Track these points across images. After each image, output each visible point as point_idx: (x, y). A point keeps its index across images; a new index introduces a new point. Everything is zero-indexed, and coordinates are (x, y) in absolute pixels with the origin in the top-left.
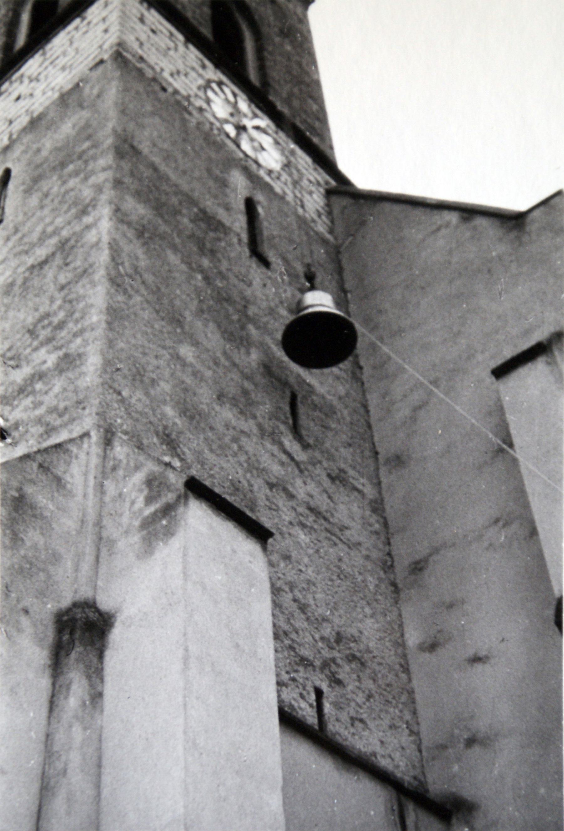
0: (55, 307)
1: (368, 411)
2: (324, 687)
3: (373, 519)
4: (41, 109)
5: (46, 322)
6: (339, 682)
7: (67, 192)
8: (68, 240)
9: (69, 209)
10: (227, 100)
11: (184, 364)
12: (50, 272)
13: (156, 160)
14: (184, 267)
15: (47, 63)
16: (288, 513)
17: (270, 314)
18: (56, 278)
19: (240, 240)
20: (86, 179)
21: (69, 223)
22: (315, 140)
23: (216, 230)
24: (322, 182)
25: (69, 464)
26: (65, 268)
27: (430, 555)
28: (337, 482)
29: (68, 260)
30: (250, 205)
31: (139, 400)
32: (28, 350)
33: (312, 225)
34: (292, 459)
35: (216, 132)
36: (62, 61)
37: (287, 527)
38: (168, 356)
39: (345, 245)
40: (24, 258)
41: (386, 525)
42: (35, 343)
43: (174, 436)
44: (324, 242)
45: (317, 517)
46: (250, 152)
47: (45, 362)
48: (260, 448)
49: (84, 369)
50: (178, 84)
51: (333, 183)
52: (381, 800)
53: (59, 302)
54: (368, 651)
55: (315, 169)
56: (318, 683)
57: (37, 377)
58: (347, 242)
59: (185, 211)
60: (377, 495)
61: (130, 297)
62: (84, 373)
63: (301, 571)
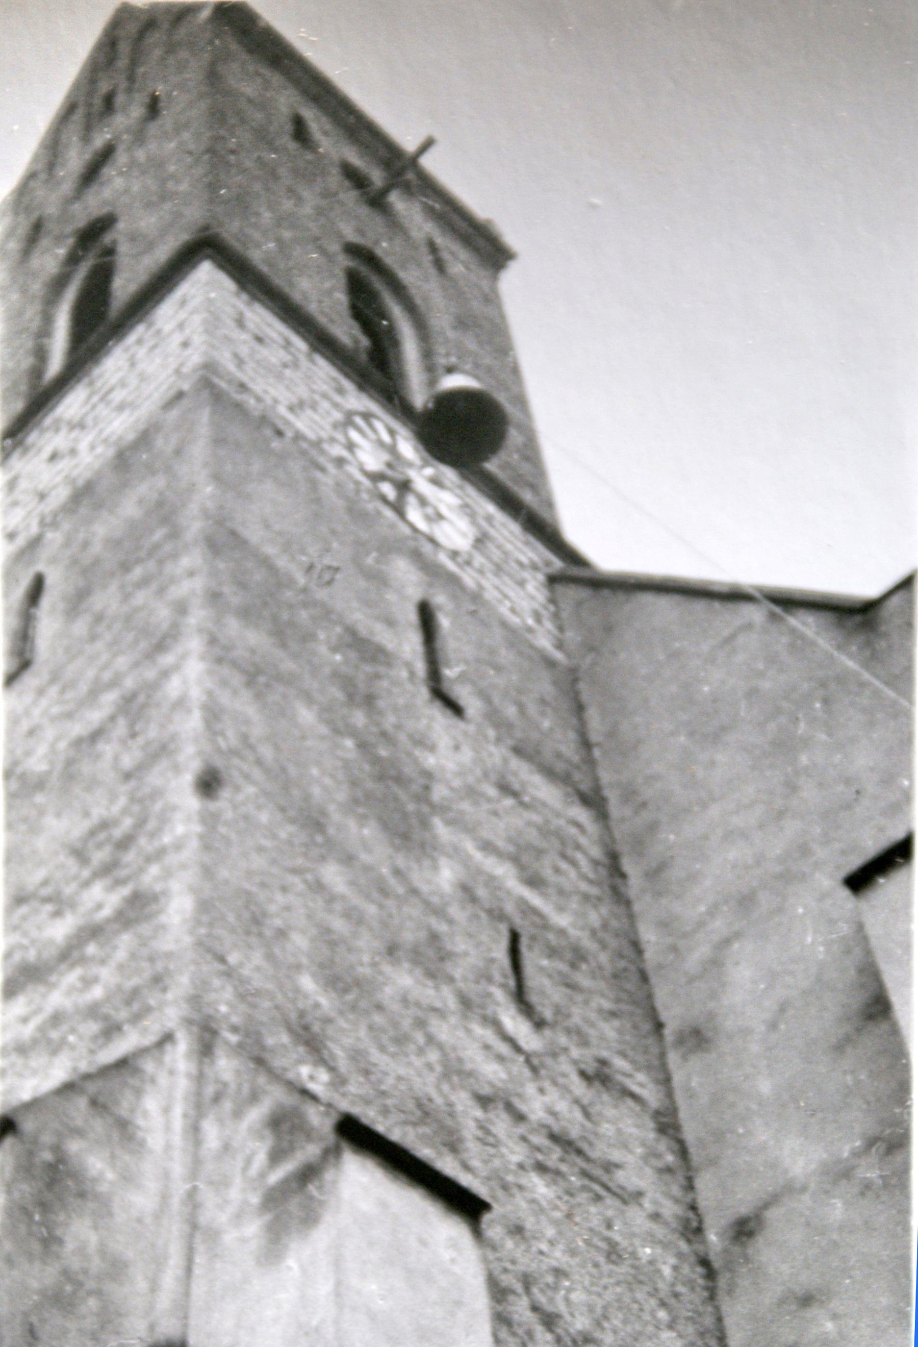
0: (116, 809)
3: (663, 1146)
4: (88, 475)
9: (136, 642)
10: (381, 443)
11: (332, 899)
12: (107, 749)
13: (270, 550)
14: (324, 730)
15: (95, 399)
19: (412, 674)
23: (373, 659)
24: (540, 563)
27: (766, 1206)
28: (597, 1084)
29: (137, 728)
31: (258, 969)
33: (529, 636)
34: (517, 1049)
35: (365, 496)
36: (118, 396)
37: (516, 1174)
41: (683, 1152)
44: (550, 664)
45: (566, 1152)
46: (422, 525)
47: (99, 906)
48: (461, 1033)
50: (302, 424)
53: (123, 801)
55: (527, 543)
59: (322, 636)
60: (667, 1102)
63: (541, 1253)
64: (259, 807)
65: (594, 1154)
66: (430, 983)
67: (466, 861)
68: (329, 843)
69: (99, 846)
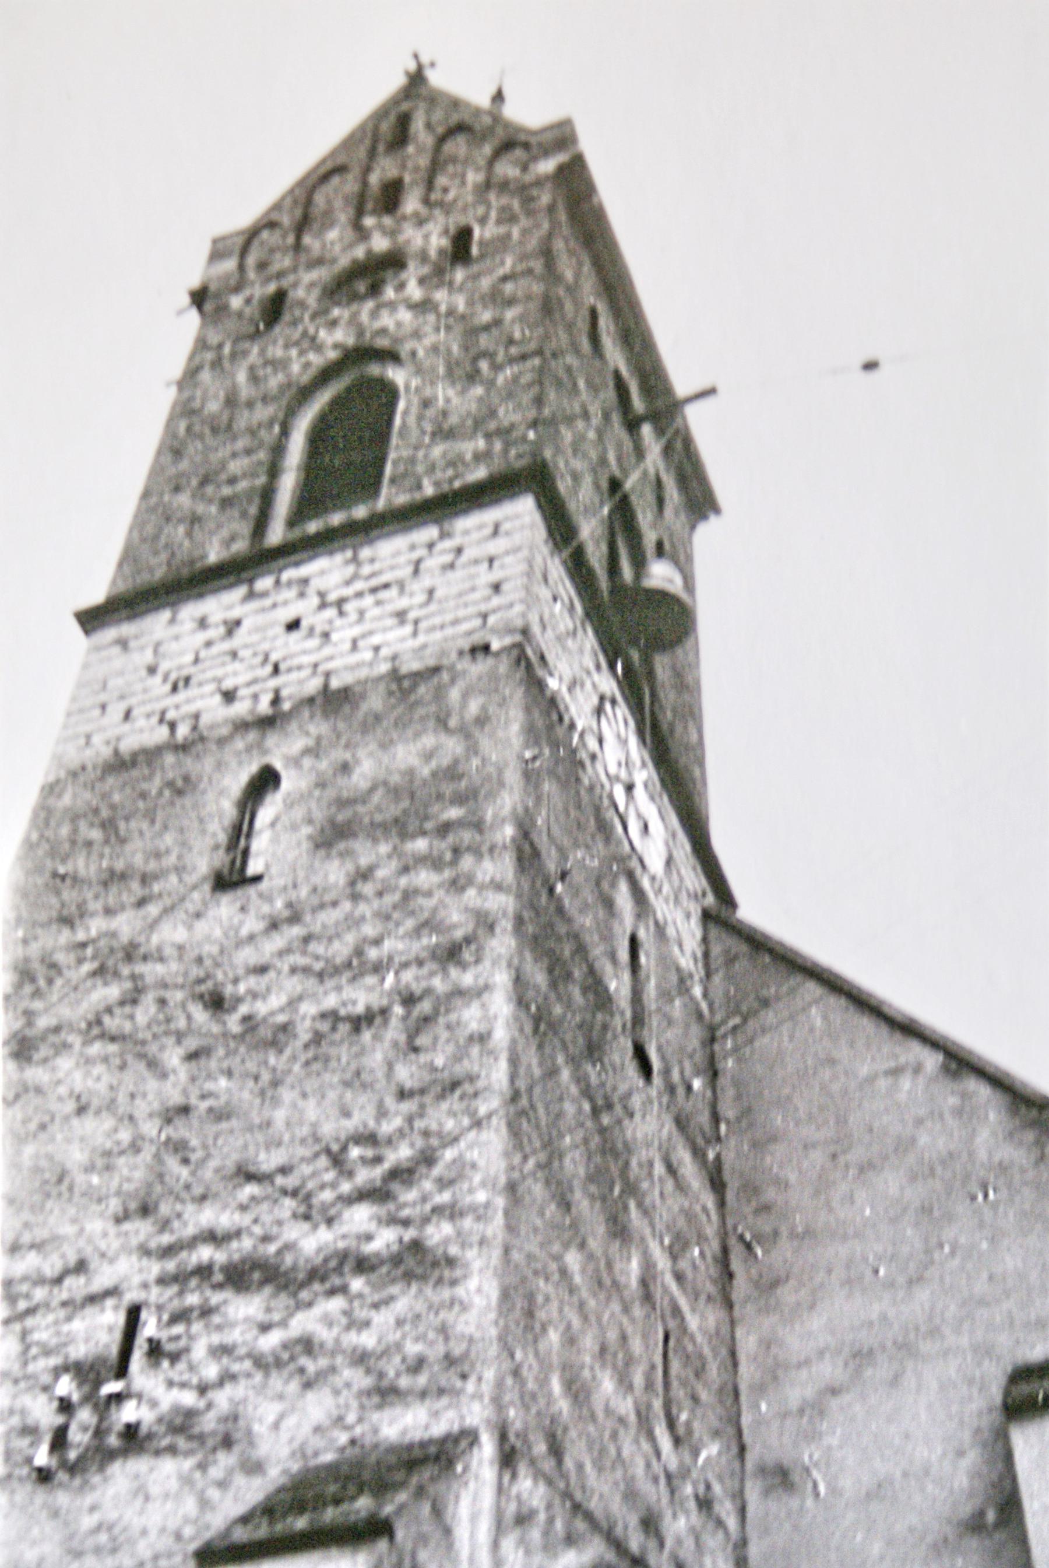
1: (735, 1364)
42: (346, 1187)
58: (731, 1023)
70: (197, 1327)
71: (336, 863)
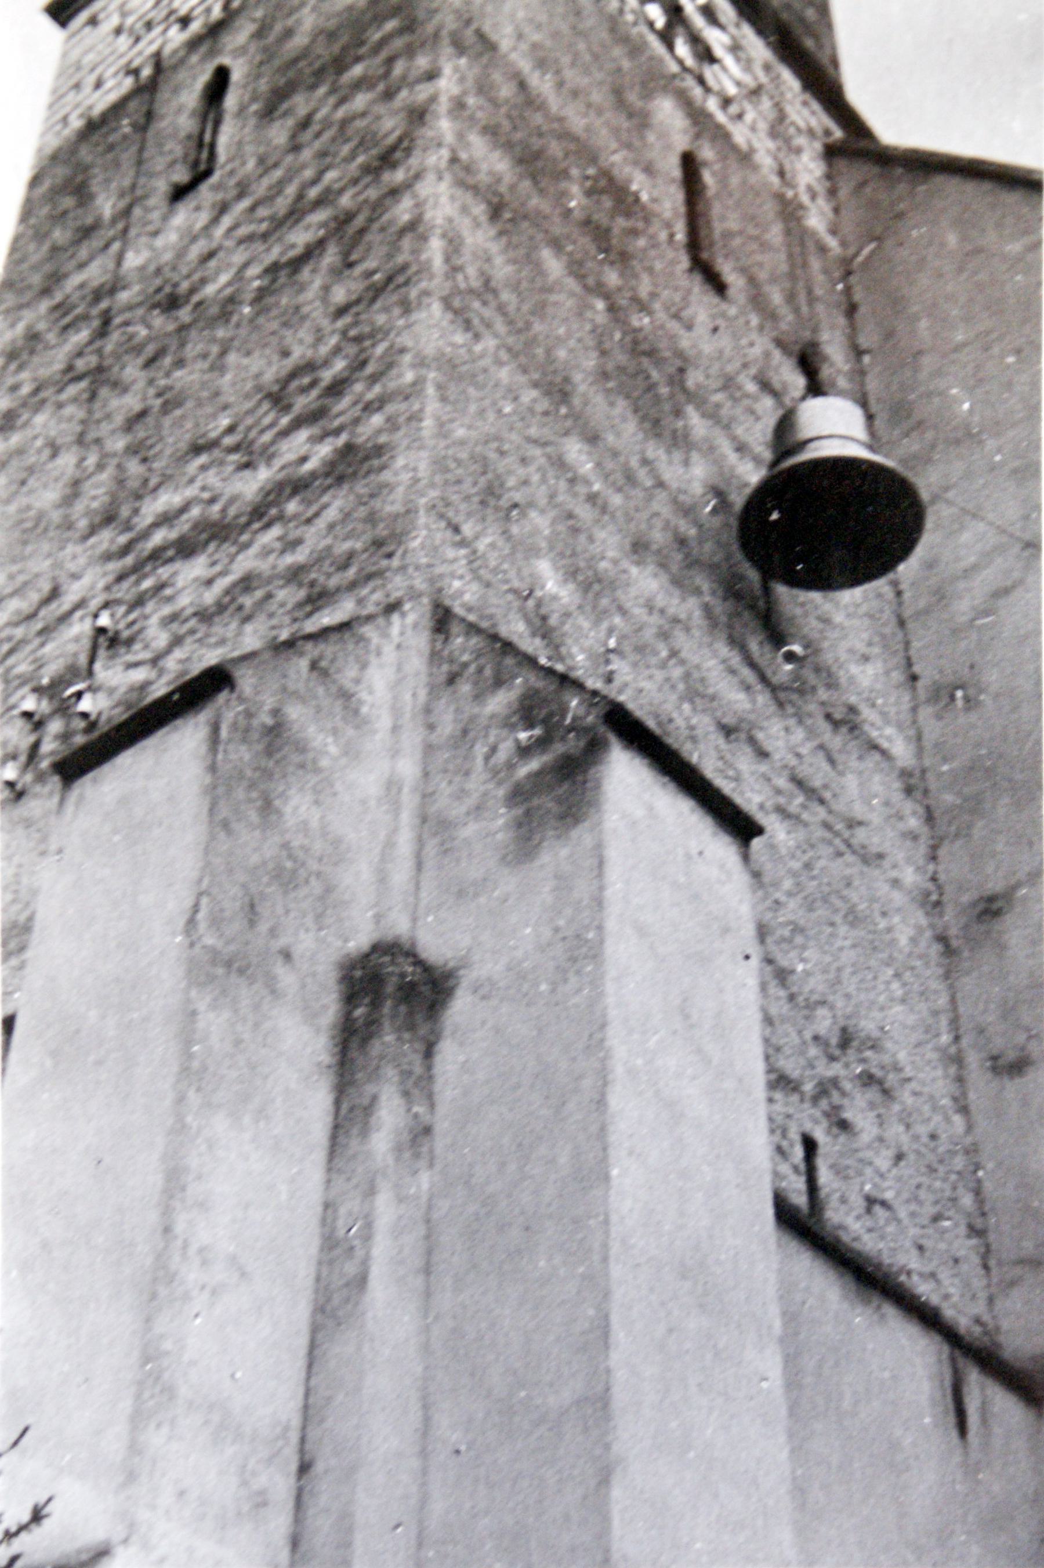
0: (324, 350)
2: (819, 1135)
5: (306, 380)
6: (844, 1125)
7: (345, 123)
8: (349, 217)
9: (352, 156)
12: (313, 278)
13: (525, 65)
14: (571, 283)
16: (757, 787)
17: (725, 388)
18: (326, 289)
20: (389, 95)
21: (355, 181)
22: (809, 43)
23: (628, 215)
24: (819, 131)
25: (364, 666)
26: (347, 273)
29: (354, 257)
30: (690, 163)
32: (267, 437)
35: (630, 18)
38: (543, 461)
39: (860, 259)
40: (259, 247)
42: (285, 421)
43: (553, 621)
47: (304, 459)
49: (386, 476)
51: (838, 134)
52: (931, 1359)
54: (897, 1068)
56: (808, 1126)
57: (288, 491)
58: (866, 252)
59: (575, 172)
61: (477, 337)
62: (386, 485)
64: (500, 363)
65: (839, 806)
66: (677, 592)
67: (719, 462)
68: (576, 416)
69: (304, 390)
70: (150, 606)
71: (277, 124)
